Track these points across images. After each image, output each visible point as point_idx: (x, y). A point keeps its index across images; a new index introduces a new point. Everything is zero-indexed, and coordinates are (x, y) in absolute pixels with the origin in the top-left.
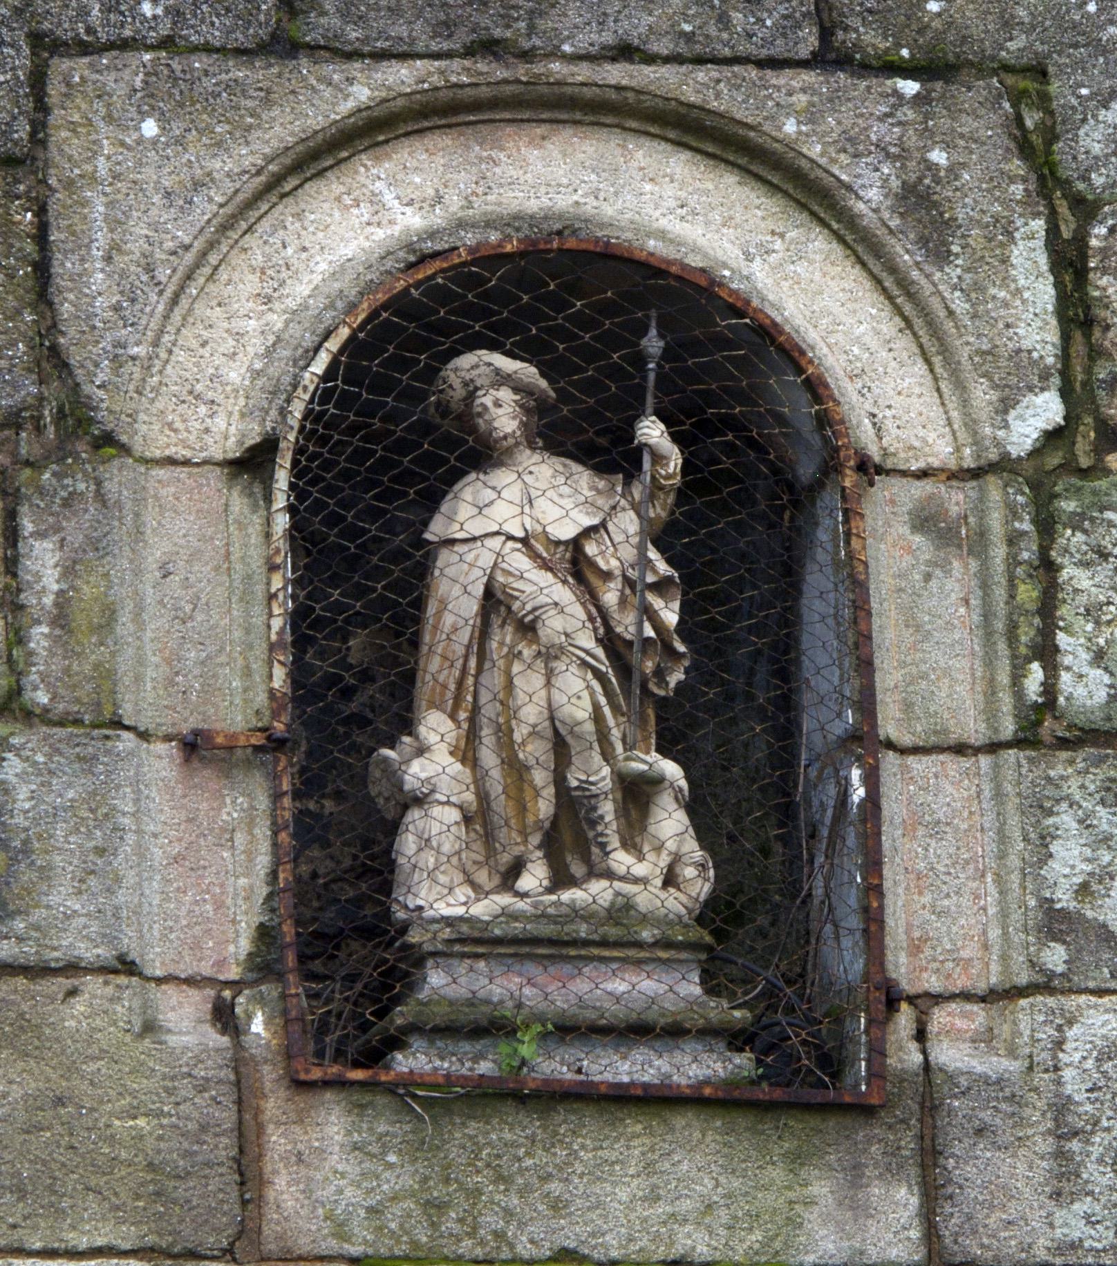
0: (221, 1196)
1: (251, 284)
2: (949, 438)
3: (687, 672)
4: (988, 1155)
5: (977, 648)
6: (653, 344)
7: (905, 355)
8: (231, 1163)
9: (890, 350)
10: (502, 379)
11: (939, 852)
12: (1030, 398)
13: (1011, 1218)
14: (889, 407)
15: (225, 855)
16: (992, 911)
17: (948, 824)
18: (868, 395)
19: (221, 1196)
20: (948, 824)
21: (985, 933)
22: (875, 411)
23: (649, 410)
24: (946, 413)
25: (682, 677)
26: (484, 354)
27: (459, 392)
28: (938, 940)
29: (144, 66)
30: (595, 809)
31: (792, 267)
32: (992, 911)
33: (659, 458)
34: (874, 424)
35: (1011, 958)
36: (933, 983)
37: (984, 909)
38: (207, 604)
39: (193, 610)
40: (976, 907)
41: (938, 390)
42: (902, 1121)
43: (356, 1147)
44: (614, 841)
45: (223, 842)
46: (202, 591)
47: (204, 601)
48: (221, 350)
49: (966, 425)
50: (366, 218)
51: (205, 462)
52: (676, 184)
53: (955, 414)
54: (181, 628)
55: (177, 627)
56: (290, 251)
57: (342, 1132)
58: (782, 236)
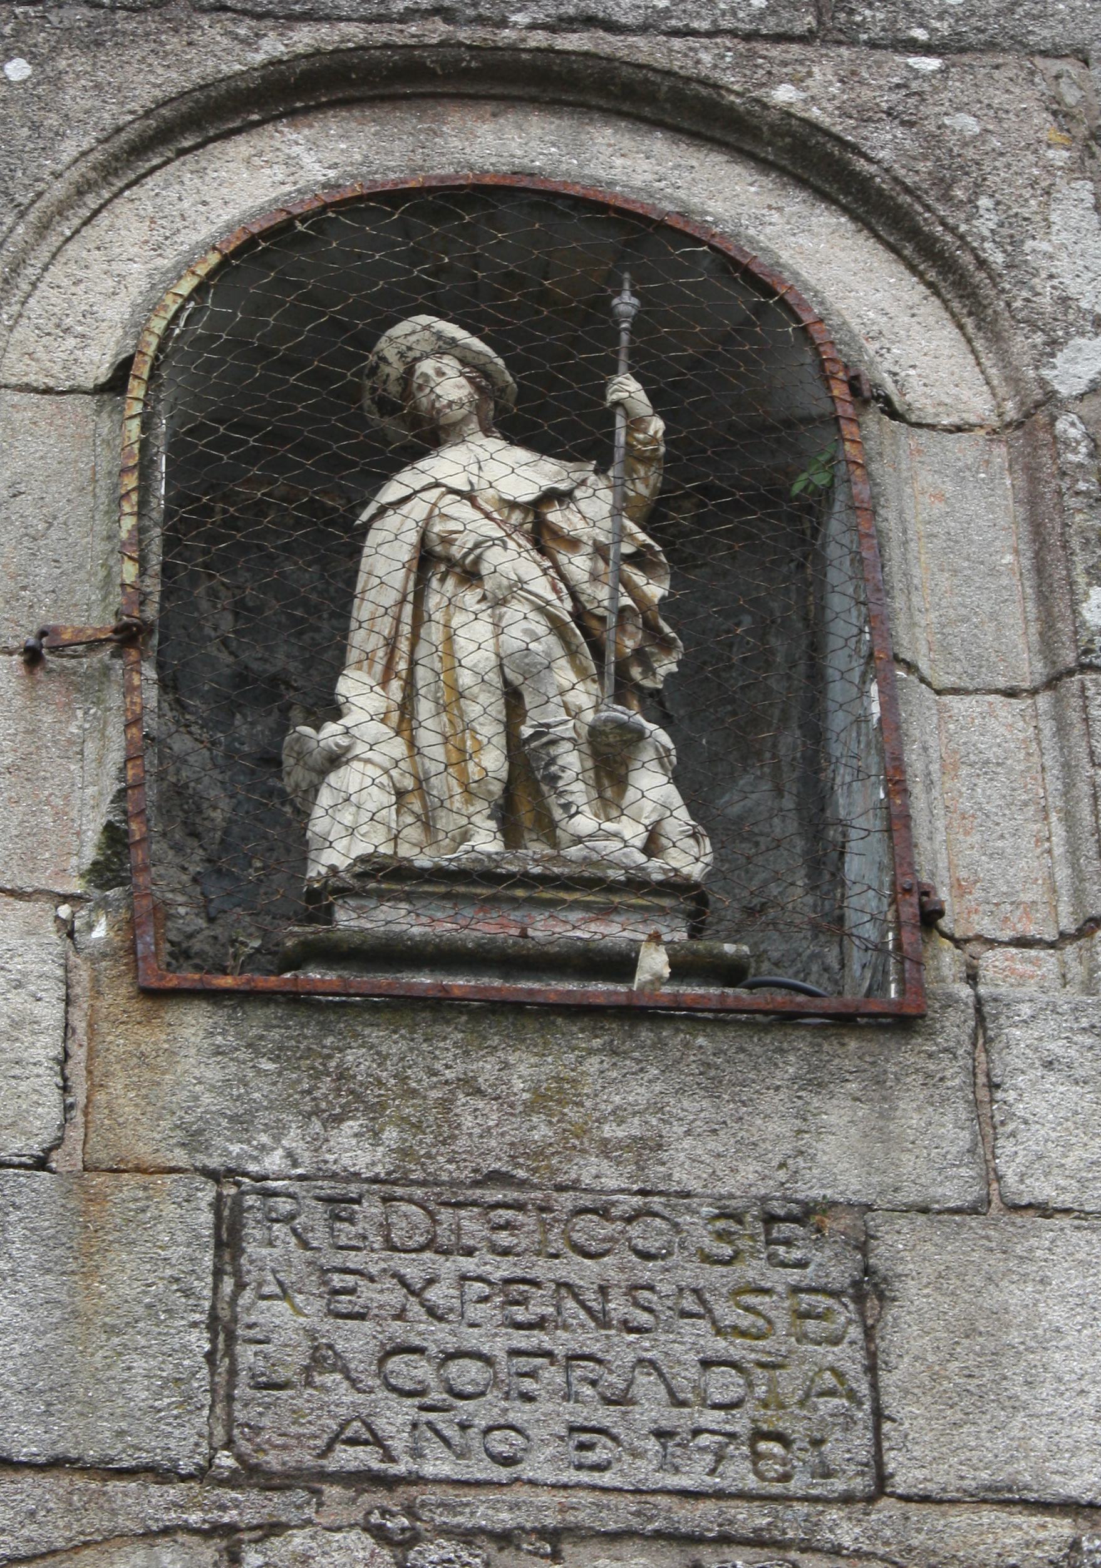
0: (35, 1097)
1: (137, 231)
2: (987, 396)
3: (679, 663)
4: (1062, 1089)
5: (1029, 591)
6: (626, 303)
7: (931, 320)
8: (51, 1064)
9: (913, 315)
10: (447, 346)
11: (988, 792)
12: (1079, 341)
13: (1095, 1157)
14: (913, 367)
15: (72, 767)
16: (1058, 851)
17: (998, 764)
18: (887, 355)
19: (35, 1097)
20: (998, 764)
21: (1051, 875)
22: (896, 369)
23: (622, 367)
24: (983, 372)
25: (674, 668)
26: (424, 319)
27: (395, 368)
28: (990, 881)
29: (16, 17)
30: (553, 761)
31: (793, 239)
32: (1058, 851)
33: (636, 424)
34: (896, 382)
35: (1084, 891)
36: (985, 926)
37: (1049, 851)
38: (65, 523)
39: (48, 528)
40: (1039, 850)
41: (973, 351)
42: (946, 1050)
43: (218, 1052)
44: (579, 792)
45: (70, 753)
46: (60, 509)
47: (61, 519)
48: (98, 289)
49: (1006, 379)
50: (280, 177)
51: (71, 391)
52: (653, 161)
53: (993, 372)
54: (31, 545)
55: (26, 544)
56: (186, 204)
57: (201, 1034)
58: (779, 209)
